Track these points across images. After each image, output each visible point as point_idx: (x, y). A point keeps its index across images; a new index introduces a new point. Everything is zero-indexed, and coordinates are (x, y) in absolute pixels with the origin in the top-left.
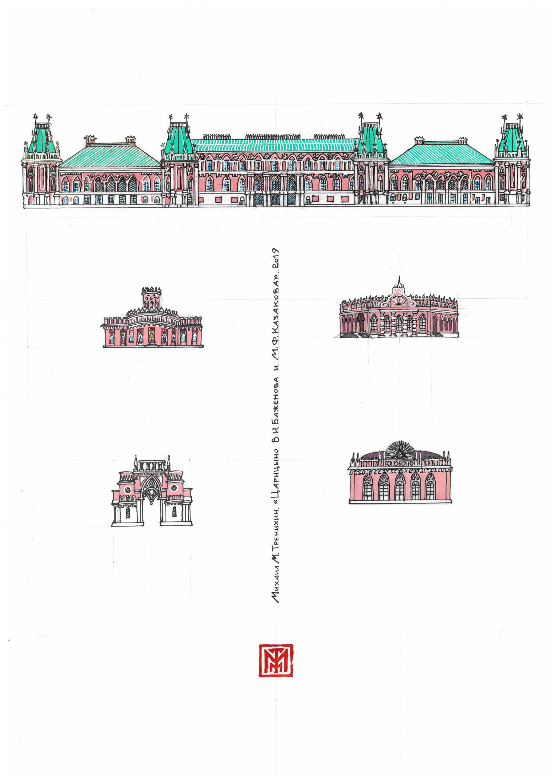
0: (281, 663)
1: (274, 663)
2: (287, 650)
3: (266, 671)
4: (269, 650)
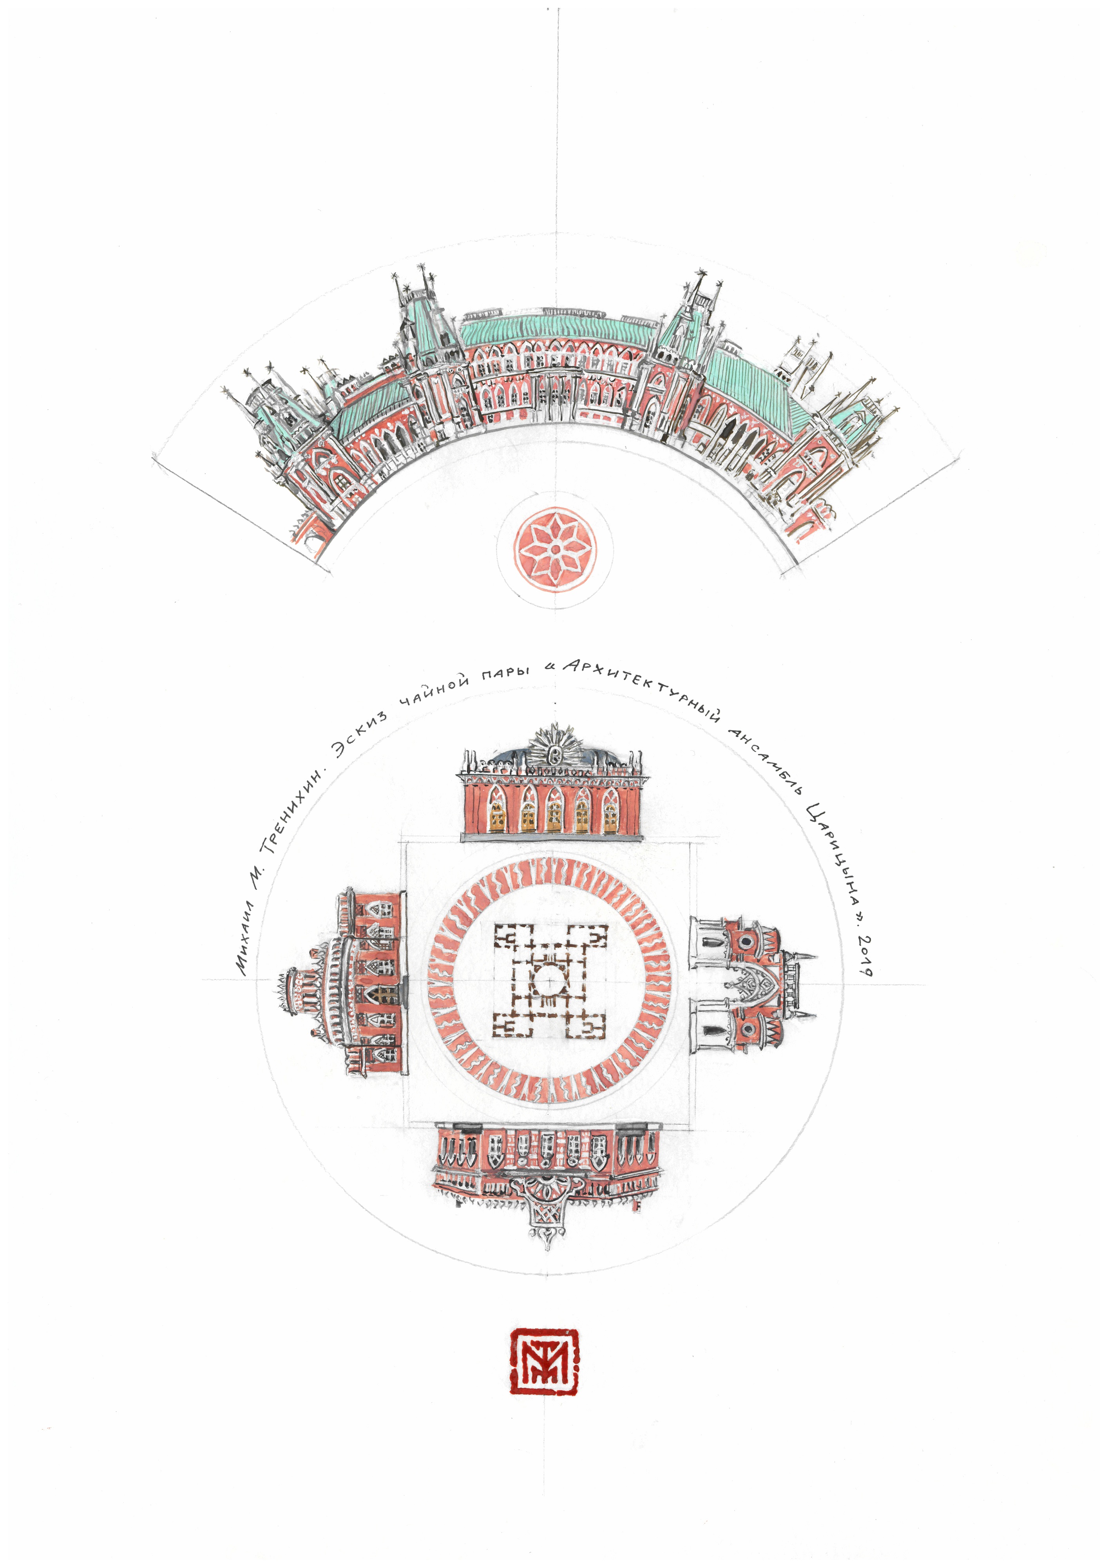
0: (556, 1368)
1: (539, 1367)
2: (566, 1345)
3: (525, 1381)
4: (533, 1343)
